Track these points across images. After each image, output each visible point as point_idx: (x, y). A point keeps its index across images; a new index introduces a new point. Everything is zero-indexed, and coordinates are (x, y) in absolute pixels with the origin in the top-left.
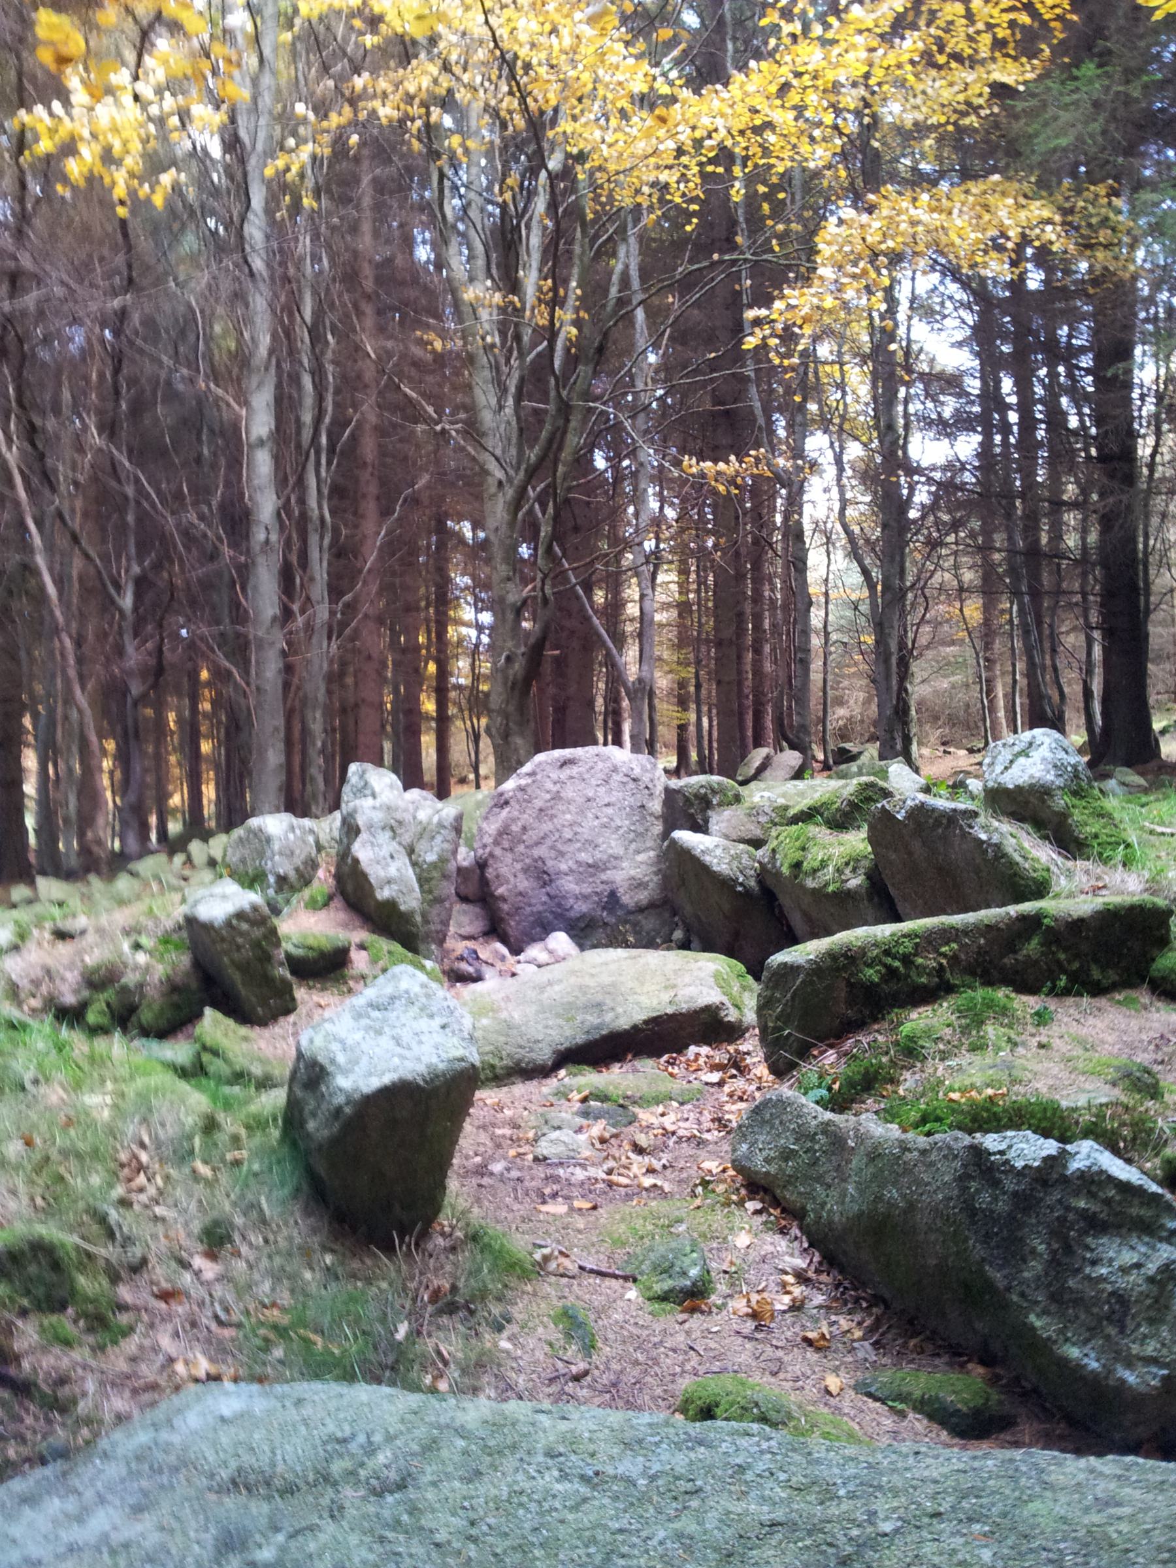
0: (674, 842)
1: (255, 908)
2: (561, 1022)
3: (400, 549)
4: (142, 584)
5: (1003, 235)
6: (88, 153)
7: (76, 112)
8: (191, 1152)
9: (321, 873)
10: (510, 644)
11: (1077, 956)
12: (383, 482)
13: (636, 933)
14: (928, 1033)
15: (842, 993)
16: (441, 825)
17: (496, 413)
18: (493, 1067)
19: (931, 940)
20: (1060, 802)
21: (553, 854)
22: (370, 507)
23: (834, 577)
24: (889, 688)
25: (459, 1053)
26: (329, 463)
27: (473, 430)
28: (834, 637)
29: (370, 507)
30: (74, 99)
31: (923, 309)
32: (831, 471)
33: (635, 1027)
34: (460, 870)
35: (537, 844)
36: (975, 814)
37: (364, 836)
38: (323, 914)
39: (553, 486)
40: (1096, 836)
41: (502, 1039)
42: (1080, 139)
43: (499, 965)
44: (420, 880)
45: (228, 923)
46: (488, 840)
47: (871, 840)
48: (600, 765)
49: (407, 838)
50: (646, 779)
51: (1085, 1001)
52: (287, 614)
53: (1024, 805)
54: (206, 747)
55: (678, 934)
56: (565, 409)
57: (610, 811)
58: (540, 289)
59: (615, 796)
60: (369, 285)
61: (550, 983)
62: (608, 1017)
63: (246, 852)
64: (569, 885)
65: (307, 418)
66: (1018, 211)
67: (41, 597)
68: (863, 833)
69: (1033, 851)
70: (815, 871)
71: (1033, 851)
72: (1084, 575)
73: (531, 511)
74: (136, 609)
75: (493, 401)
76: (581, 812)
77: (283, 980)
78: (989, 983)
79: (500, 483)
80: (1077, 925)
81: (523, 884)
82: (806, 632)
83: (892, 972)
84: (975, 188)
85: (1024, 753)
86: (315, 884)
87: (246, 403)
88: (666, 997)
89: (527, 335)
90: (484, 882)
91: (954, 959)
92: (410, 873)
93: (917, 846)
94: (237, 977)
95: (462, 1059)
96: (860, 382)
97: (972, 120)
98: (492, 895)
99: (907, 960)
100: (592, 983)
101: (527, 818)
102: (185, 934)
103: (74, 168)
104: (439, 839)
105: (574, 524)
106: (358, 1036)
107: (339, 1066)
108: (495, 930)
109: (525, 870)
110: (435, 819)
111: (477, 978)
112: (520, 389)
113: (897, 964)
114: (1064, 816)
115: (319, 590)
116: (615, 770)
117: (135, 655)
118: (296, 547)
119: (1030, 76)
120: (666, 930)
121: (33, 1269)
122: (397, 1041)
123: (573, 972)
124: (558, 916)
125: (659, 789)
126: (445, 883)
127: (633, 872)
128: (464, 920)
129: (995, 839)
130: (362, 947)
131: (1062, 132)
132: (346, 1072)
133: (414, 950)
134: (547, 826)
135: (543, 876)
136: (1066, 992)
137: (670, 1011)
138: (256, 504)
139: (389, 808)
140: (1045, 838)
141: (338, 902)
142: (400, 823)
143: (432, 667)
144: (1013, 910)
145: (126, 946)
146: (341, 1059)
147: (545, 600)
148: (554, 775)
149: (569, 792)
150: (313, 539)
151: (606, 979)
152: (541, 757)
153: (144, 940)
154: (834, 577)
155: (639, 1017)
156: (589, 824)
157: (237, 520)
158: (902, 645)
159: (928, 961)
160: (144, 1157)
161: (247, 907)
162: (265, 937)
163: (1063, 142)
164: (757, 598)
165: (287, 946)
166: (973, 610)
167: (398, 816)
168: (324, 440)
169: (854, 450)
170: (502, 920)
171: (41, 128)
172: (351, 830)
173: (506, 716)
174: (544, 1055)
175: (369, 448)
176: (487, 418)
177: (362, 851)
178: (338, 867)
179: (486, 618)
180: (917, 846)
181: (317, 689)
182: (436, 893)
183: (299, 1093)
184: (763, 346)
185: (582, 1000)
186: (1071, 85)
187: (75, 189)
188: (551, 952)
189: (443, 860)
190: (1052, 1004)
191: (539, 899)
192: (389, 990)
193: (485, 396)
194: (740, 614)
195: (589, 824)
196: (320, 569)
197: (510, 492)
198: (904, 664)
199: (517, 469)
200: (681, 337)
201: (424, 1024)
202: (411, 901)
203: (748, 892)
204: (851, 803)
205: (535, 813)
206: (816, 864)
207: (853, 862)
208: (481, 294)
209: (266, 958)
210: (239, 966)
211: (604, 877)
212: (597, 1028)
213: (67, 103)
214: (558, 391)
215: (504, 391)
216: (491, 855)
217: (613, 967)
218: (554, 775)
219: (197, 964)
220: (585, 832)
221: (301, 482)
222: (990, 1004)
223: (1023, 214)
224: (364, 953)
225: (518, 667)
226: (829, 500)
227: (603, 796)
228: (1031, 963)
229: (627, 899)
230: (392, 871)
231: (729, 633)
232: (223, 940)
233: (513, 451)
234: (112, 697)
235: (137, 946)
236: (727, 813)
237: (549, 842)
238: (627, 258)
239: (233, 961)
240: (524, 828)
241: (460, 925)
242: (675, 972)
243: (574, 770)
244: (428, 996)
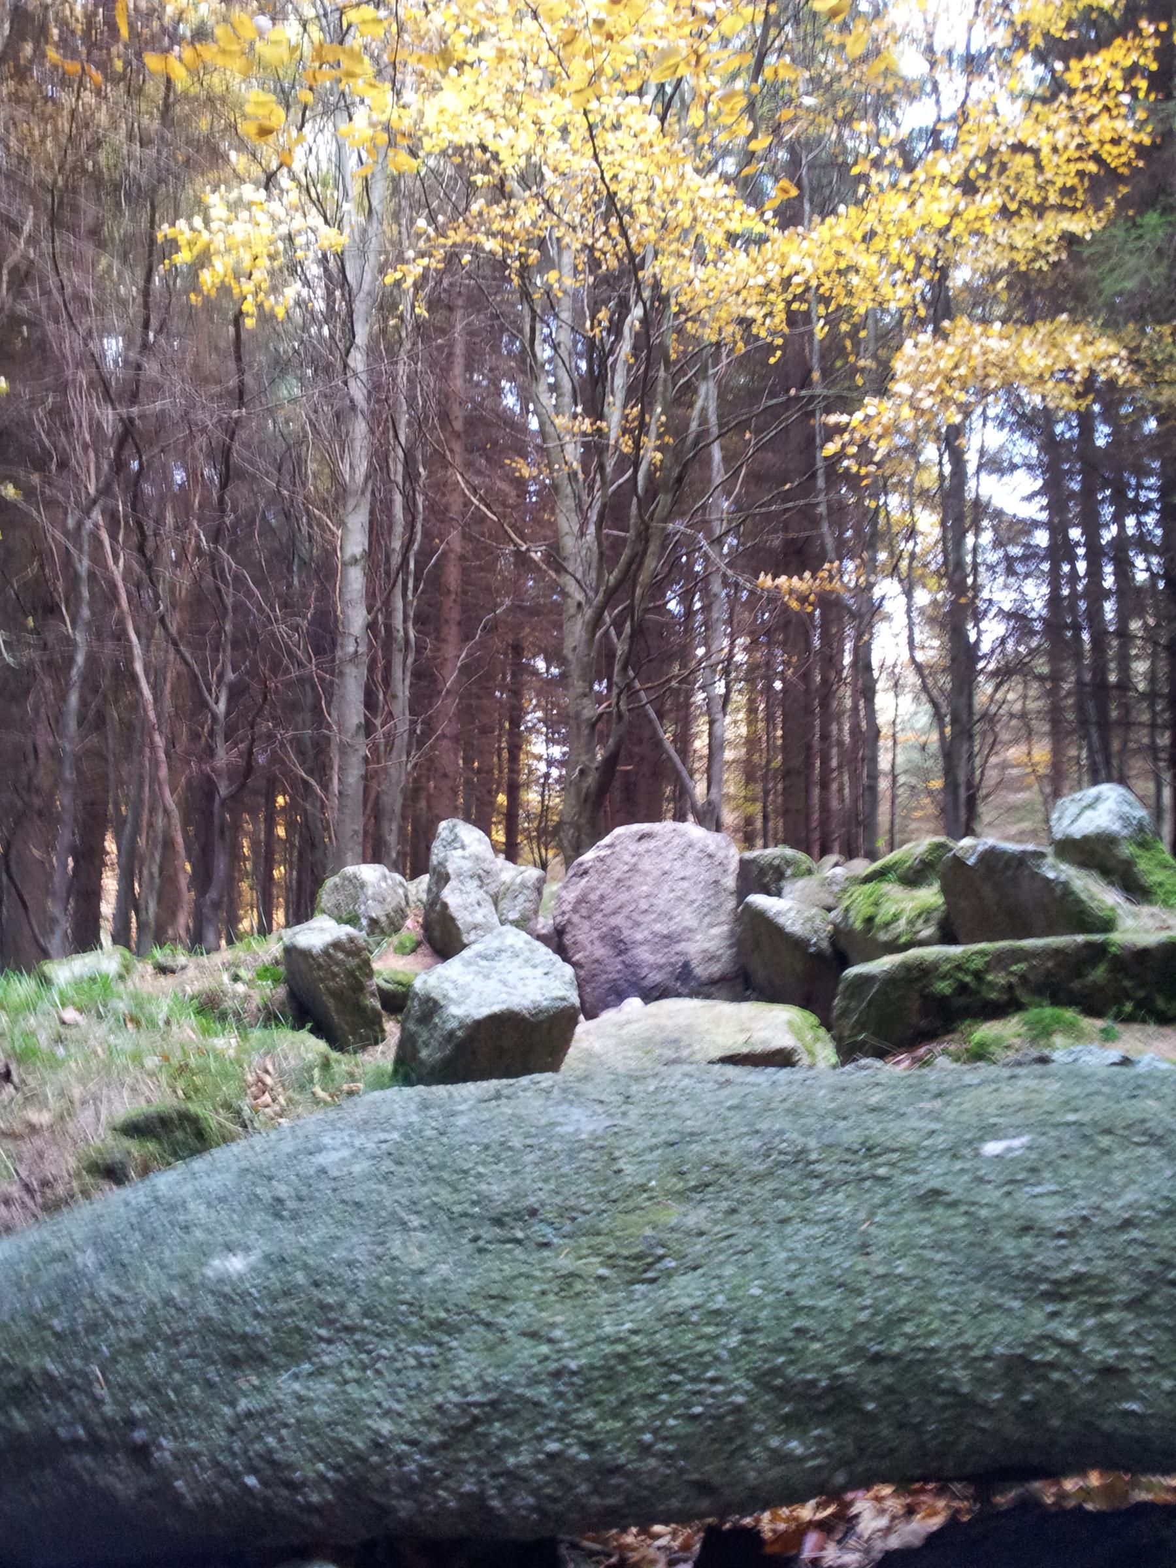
0: (748, 906)
1: (351, 940)
2: (639, 1053)
4: (236, 693)
5: (1071, 369)
6: (220, 265)
7: (214, 226)
8: (311, 1081)
9: (409, 923)
11: (1142, 985)
12: (465, 608)
14: (998, 1041)
15: (915, 1004)
16: (523, 885)
17: (578, 538)
19: (1000, 960)
20: (1127, 850)
21: (629, 924)
22: (452, 633)
23: (902, 716)
24: (957, 819)
25: (561, 994)
26: (415, 589)
27: (555, 558)
28: (902, 779)
29: (452, 633)
30: (214, 213)
31: (994, 464)
32: (901, 620)
36: (1042, 855)
37: (453, 883)
38: (411, 958)
39: (630, 609)
40: (1161, 885)
42: (1146, 282)
45: (325, 952)
46: (567, 907)
47: (944, 890)
48: (676, 841)
49: (493, 888)
50: (720, 855)
51: (1152, 1028)
52: (368, 728)
53: (1093, 853)
54: (279, 872)
56: (644, 537)
57: (685, 884)
58: (625, 417)
59: (689, 871)
60: (458, 425)
63: (341, 898)
64: (644, 955)
65: (397, 545)
66: (1086, 349)
67: (136, 705)
68: (936, 886)
69: (1103, 896)
70: (887, 925)
71: (1103, 896)
72: (1152, 706)
73: (607, 632)
74: (228, 713)
75: (576, 528)
76: (658, 884)
77: (374, 1009)
78: (1056, 1002)
79: (579, 605)
80: (1142, 955)
81: (600, 951)
82: (874, 775)
83: (963, 988)
84: (1044, 328)
85: (1090, 806)
86: (404, 932)
87: (341, 524)
88: (742, 1038)
89: (610, 463)
91: (1023, 978)
93: (987, 891)
94: (331, 1003)
95: (563, 999)
96: (928, 522)
97: (1040, 264)
99: (978, 975)
100: (669, 1023)
101: (605, 888)
102: (282, 969)
103: (207, 278)
104: (521, 898)
105: (645, 657)
106: (469, 978)
107: (451, 1000)
109: (602, 938)
112: (601, 516)
113: (968, 979)
114: (1129, 863)
115: (401, 706)
117: (224, 756)
118: (381, 664)
119: (1097, 227)
121: (179, 1135)
122: (504, 983)
125: (734, 865)
127: (706, 945)
129: (1063, 878)
131: (1128, 276)
132: (459, 1004)
134: (623, 897)
135: (618, 944)
136: (1129, 1019)
138: (346, 617)
140: (1111, 883)
141: (425, 949)
143: (502, 799)
144: (1080, 938)
145: (226, 978)
146: (453, 994)
147: (620, 716)
149: (646, 865)
150: (398, 658)
152: (619, 830)
153: (242, 973)
154: (902, 716)
156: (664, 898)
157: (325, 634)
158: (970, 785)
159: (998, 978)
160: (269, 1080)
161: (344, 938)
162: (359, 968)
163: (1130, 285)
164: (825, 737)
165: (378, 981)
166: (1041, 752)
167: (486, 866)
168: (412, 566)
169: (922, 597)
171: (182, 240)
172: (442, 878)
173: (578, 829)
175: (453, 576)
176: (569, 544)
177: (451, 897)
178: (426, 916)
179: (557, 751)
180: (987, 891)
181: (394, 801)
183: (412, 1027)
184: (840, 455)
185: (658, 1038)
186: (1134, 233)
187: (207, 298)
190: (1119, 1027)
191: (615, 966)
192: (496, 944)
193: (567, 523)
194: (809, 747)
196: (402, 687)
197: (589, 613)
198: (971, 802)
200: (756, 478)
201: (527, 972)
203: (819, 954)
204: (922, 861)
205: (612, 882)
206: (888, 918)
207: (925, 914)
208: (571, 425)
209: (359, 988)
210: (332, 993)
211: (679, 947)
213: (207, 222)
214: (639, 516)
215: (586, 519)
218: (633, 847)
219: (292, 995)
220: (661, 903)
221: (387, 602)
222: (1058, 1020)
223: (1090, 350)
225: (591, 780)
226: (898, 640)
227: (679, 869)
228: (1097, 988)
230: (479, 917)
231: (797, 762)
232: (320, 967)
233: (593, 575)
234: (200, 802)
235: (236, 978)
236: (801, 883)
237: (625, 912)
238: (707, 395)
239: (327, 988)
240: (602, 898)
243: (651, 844)
244: (532, 951)
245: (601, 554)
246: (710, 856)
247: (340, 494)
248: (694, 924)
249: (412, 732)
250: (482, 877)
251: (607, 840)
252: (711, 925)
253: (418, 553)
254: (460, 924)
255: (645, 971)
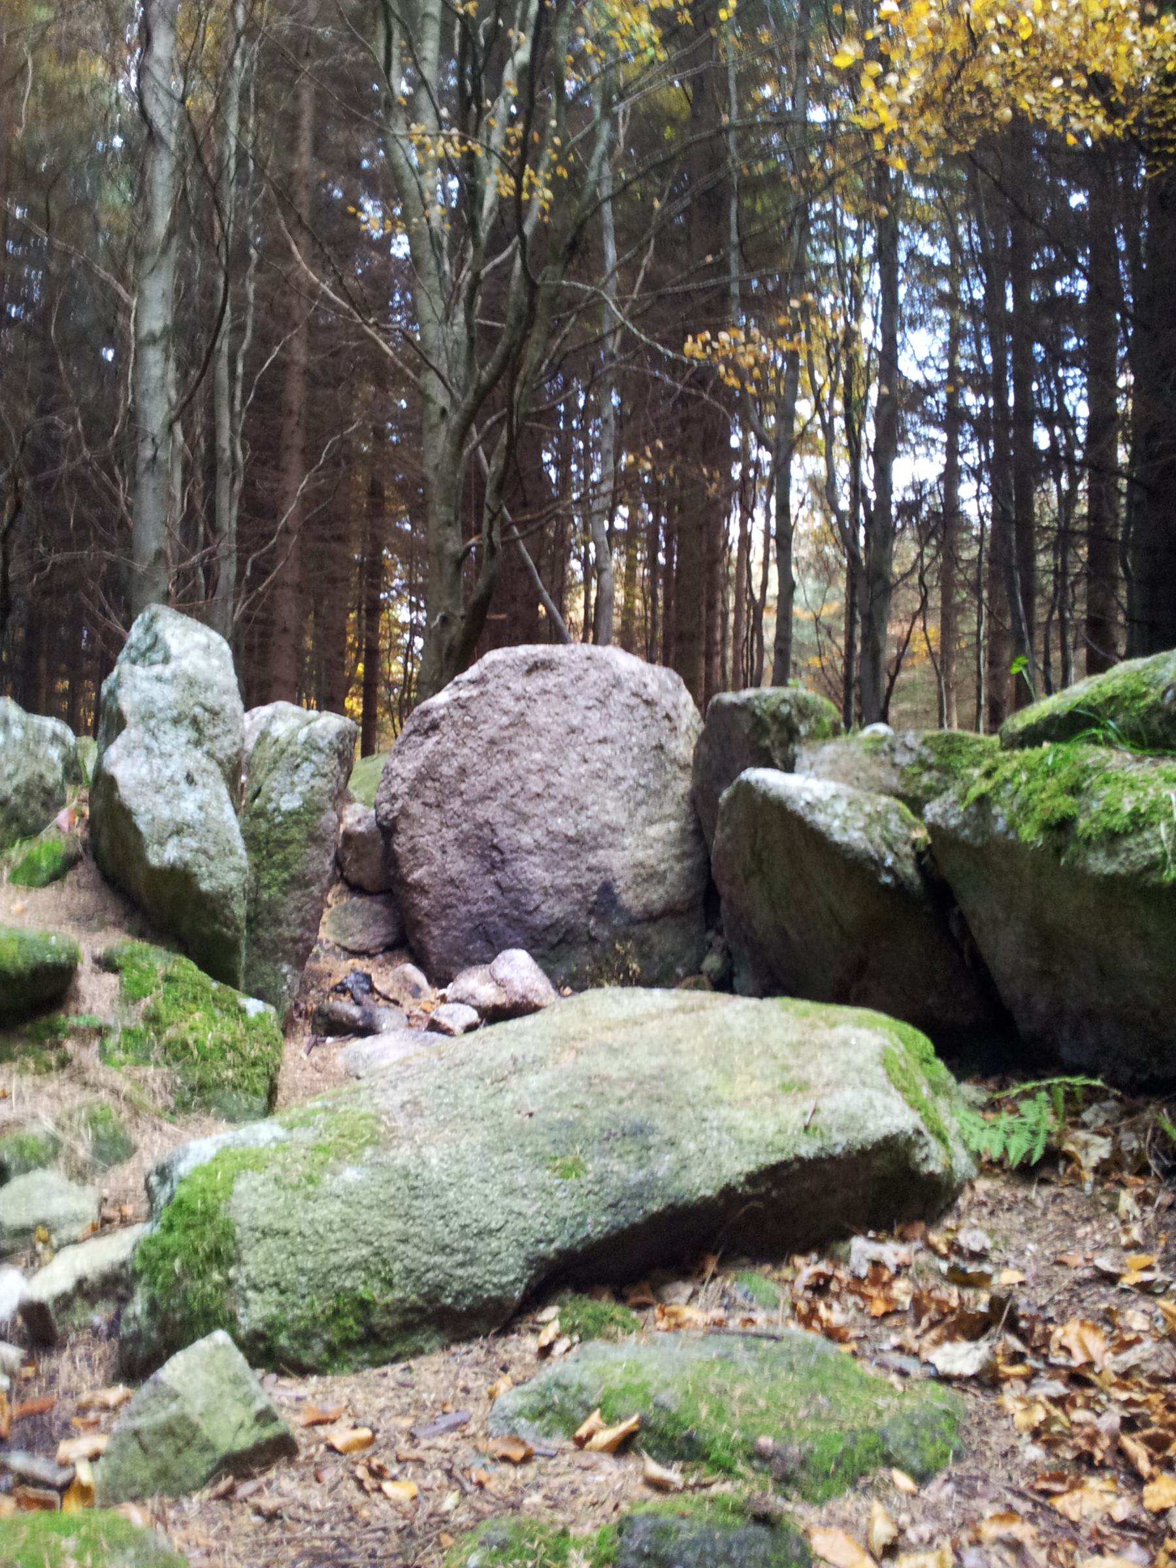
2: (544, 1176)
3: (325, 518)
10: (447, 602)
13: (643, 956)
16: (311, 745)
17: (438, 327)
18: (364, 1305)
21: (509, 817)
22: (293, 461)
33: (728, 1192)
34: (348, 837)
35: (483, 798)
37: (132, 734)
38: (46, 895)
41: (395, 1226)
43: (408, 1003)
44: (252, 840)
46: (399, 787)
48: (593, 675)
50: (666, 702)
55: (712, 962)
57: (606, 751)
61: (518, 1067)
62: (663, 1165)
64: (534, 871)
70: (1113, 837)
75: (440, 313)
76: (559, 750)
79: (443, 412)
81: (458, 865)
86: (48, 836)
88: (793, 1113)
90: (391, 859)
92: (228, 818)
98: (402, 882)
100: (612, 1068)
104: (307, 769)
108: (404, 941)
110: (302, 735)
111: (367, 1030)
116: (617, 684)
120: (690, 955)
123: (567, 1041)
124: (514, 922)
126: (313, 851)
127: (641, 855)
128: (340, 924)
130: (107, 964)
133: (226, 976)
134: (501, 770)
135: (491, 853)
137: (807, 1149)
139: (191, 682)
141: (84, 873)
142: (214, 713)
148: (517, 686)
149: (540, 716)
150: (224, 483)
151: (648, 1063)
155: (737, 1165)
156: (570, 773)
167: (211, 699)
170: (418, 924)
174: (503, 1270)
175: (295, 392)
182: (297, 868)
188: (500, 984)
189: (312, 808)
195: (571, 770)
196: (229, 515)
197: (455, 418)
199: (465, 391)
202: (226, 871)
211: (592, 860)
212: (639, 1192)
216: (404, 813)
217: (653, 1029)
218: (517, 686)
220: (565, 784)
224: (110, 979)
225: (456, 630)
229: (628, 899)
230: (188, 807)
233: (461, 370)
237: (502, 797)
240: (463, 771)
241: (344, 930)
242: (796, 1047)
243: (550, 680)
245: (471, 340)
246: (649, 703)
247: (131, 256)
248: (621, 818)
249: (240, 574)
250: (199, 724)
251: (473, 672)
252: (650, 822)
253: (246, 355)
254: (142, 823)
255: (537, 898)
